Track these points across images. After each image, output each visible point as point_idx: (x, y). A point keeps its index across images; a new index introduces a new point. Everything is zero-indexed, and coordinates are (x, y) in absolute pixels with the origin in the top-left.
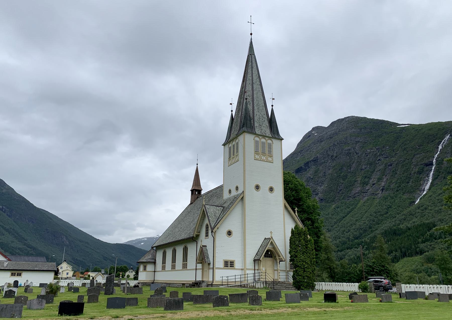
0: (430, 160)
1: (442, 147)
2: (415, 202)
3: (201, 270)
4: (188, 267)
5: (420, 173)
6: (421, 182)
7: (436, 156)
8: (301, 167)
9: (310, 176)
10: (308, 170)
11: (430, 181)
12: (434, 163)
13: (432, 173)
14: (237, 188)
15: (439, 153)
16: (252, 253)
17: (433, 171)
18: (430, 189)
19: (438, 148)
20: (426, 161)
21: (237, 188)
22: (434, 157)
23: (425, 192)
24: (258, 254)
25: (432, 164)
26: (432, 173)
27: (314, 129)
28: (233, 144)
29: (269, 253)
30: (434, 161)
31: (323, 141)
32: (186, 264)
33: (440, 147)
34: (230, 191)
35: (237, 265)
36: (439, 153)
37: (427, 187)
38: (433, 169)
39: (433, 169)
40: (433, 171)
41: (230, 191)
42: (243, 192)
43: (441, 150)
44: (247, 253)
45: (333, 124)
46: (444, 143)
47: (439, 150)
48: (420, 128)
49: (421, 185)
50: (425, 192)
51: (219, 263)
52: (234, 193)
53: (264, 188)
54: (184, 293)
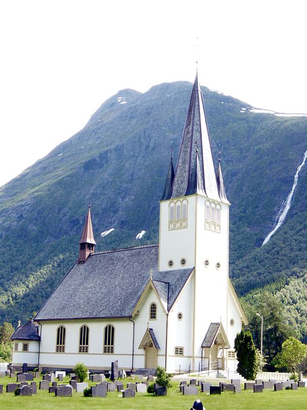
2: (263, 240)
3: (143, 357)
5: (274, 193)
6: (276, 209)
7: (300, 168)
8: (94, 160)
9: (107, 177)
10: (105, 165)
11: (288, 207)
12: (296, 180)
13: (291, 194)
14: (183, 262)
16: (199, 341)
17: (292, 192)
18: (285, 222)
21: (183, 262)
22: (297, 170)
25: (292, 181)
26: (291, 194)
27: (121, 93)
28: (179, 203)
29: (213, 341)
30: (296, 176)
31: (134, 117)
32: (64, 347)
34: (171, 263)
35: (185, 352)
37: (282, 217)
38: (294, 188)
39: (294, 188)
40: (292, 192)
41: (171, 263)
42: (194, 267)
45: (154, 90)
49: (275, 213)
51: (171, 351)
52: (177, 266)
53: (212, 264)
54: (304, 383)
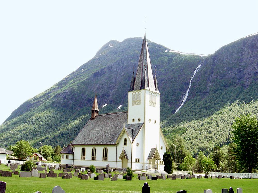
0: (188, 80)
1: (196, 72)
2: (176, 111)
3: (121, 163)
4: (85, 158)
8: (98, 72)
9: (105, 80)
11: (187, 96)
13: (188, 90)
14: (139, 120)
15: (194, 76)
17: (189, 89)
19: (193, 72)
20: (185, 81)
21: (139, 120)
23: (182, 104)
24: (150, 156)
30: (191, 82)
33: (195, 72)
34: (133, 120)
36: (194, 76)
37: (184, 100)
38: (189, 87)
40: (189, 89)
41: (133, 120)
42: (144, 122)
43: (195, 74)
44: (145, 156)
45: (126, 41)
46: (197, 69)
47: (194, 74)
48: (184, 56)
49: (181, 99)
50: (182, 104)
51: (134, 160)
